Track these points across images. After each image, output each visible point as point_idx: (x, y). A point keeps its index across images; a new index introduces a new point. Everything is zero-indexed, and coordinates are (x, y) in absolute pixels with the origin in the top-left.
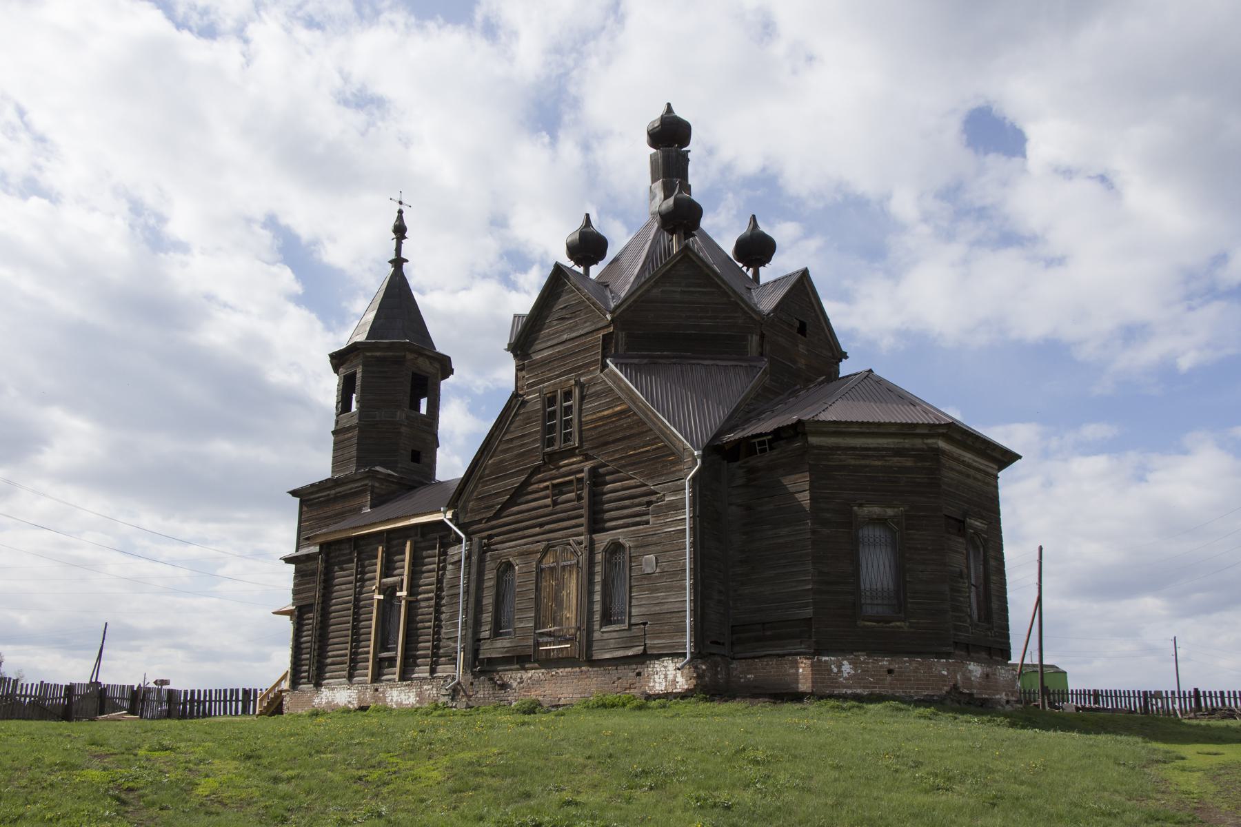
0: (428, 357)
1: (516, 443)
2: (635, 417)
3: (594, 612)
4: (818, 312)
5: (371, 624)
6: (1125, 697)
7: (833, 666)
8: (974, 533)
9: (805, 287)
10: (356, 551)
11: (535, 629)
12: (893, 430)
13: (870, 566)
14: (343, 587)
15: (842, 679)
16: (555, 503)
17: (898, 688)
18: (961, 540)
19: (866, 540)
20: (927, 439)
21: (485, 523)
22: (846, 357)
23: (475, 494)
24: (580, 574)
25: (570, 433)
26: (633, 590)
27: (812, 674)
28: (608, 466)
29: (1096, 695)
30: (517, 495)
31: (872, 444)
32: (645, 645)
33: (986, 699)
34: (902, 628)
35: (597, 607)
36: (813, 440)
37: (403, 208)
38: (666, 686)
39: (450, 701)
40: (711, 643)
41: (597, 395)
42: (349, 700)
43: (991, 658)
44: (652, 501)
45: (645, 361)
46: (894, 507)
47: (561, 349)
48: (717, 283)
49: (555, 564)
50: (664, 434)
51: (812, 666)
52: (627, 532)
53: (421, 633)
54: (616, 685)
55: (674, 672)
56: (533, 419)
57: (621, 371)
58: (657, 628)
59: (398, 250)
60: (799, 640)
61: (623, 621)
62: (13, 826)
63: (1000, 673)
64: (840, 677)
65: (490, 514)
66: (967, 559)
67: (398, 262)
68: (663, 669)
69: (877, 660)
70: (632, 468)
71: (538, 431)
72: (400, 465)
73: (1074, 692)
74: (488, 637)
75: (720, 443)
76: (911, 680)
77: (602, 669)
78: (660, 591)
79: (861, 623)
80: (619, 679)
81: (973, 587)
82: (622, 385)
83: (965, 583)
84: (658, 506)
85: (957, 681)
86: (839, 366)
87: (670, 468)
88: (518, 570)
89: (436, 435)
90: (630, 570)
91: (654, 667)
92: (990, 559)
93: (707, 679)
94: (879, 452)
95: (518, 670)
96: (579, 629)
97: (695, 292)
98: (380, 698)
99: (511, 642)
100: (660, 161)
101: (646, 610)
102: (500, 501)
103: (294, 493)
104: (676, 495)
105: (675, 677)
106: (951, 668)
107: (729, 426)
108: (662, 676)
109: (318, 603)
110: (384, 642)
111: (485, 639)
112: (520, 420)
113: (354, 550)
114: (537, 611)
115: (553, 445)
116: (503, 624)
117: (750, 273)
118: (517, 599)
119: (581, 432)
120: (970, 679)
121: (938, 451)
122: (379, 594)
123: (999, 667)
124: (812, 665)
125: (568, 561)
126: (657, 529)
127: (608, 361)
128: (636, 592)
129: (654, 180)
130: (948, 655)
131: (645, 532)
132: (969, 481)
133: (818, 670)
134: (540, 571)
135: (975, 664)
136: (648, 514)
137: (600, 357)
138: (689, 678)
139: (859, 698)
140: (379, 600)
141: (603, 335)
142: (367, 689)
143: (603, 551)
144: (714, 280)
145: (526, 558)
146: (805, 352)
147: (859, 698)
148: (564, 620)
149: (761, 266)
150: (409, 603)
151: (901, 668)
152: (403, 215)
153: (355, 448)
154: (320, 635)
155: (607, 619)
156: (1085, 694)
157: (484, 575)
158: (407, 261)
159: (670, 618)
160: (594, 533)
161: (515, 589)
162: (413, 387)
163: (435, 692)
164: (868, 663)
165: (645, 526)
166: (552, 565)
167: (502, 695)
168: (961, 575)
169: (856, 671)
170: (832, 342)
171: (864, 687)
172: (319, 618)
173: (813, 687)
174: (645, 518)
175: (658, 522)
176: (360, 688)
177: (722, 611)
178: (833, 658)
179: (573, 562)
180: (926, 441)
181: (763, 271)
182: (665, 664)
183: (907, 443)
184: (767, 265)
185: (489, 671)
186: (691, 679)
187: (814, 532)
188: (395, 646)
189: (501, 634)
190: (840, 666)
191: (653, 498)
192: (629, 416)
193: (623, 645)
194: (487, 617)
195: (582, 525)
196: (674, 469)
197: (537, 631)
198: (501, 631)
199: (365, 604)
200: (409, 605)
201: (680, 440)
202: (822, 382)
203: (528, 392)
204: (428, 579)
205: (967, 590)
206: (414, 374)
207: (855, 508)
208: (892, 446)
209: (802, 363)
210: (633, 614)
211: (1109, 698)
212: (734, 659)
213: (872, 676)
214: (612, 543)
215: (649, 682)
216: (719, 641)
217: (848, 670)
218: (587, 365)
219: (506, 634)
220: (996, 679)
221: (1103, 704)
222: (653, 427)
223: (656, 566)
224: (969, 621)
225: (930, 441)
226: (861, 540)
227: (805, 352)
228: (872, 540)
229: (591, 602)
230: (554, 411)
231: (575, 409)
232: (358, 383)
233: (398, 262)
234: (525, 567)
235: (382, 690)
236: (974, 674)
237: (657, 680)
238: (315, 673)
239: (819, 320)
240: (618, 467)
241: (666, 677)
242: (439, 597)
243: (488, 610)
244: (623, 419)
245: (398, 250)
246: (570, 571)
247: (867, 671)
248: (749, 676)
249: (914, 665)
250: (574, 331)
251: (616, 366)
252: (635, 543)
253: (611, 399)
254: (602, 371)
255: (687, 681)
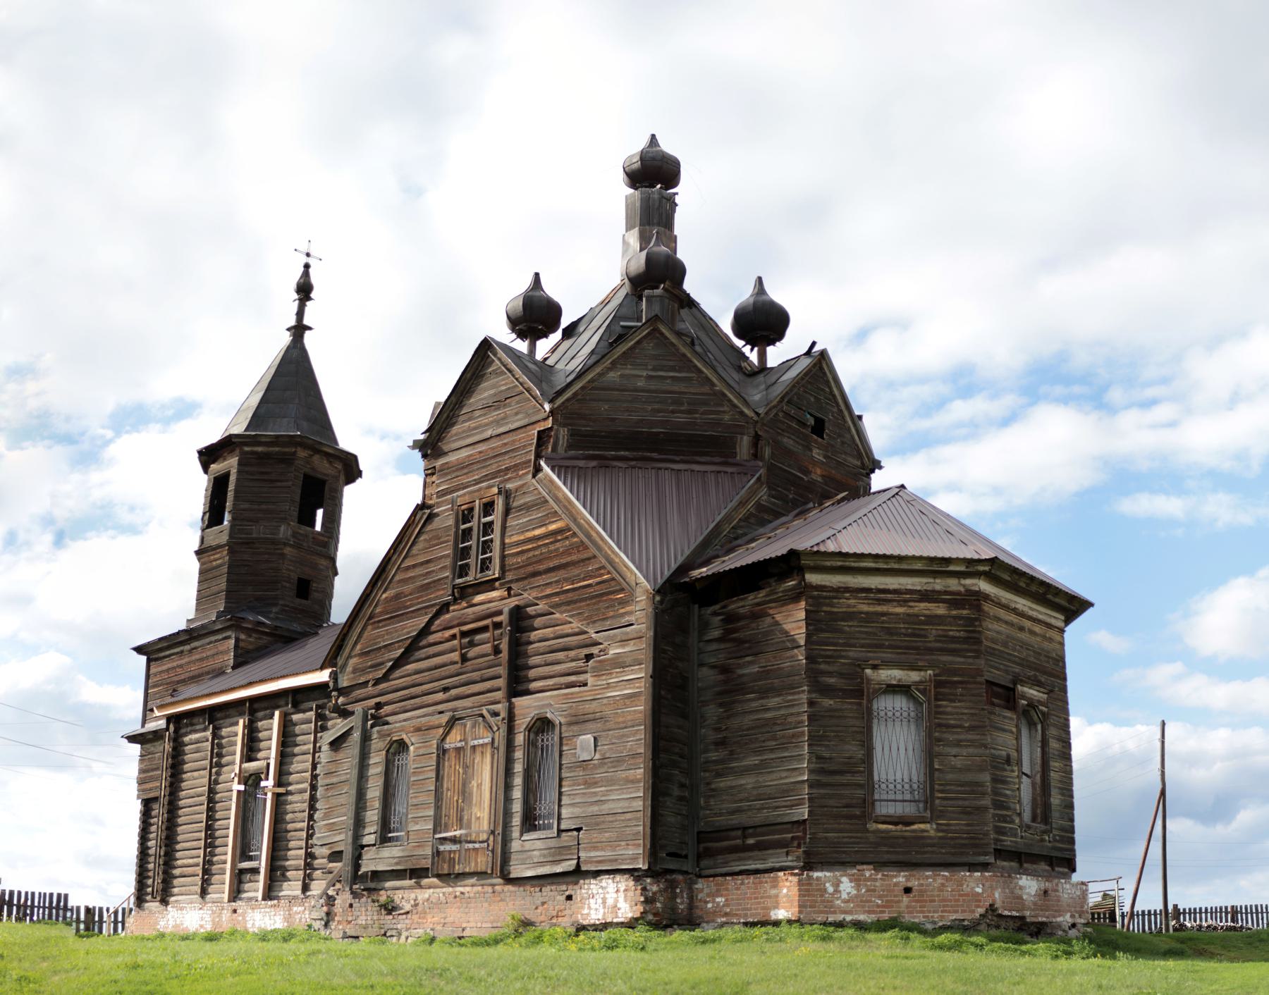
0: (327, 455)
1: (418, 571)
2: (576, 539)
3: (512, 813)
4: (843, 407)
5: (229, 824)
6: (1252, 913)
7: (827, 885)
8: (1028, 705)
9: (825, 374)
10: (211, 726)
11: (435, 832)
12: (918, 566)
13: (887, 749)
14: (196, 774)
15: (839, 902)
16: (464, 659)
17: (917, 912)
18: (1008, 714)
19: (882, 714)
20: (964, 578)
21: (374, 685)
22: (880, 468)
23: (358, 647)
24: (496, 756)
25: (490, 559)
26: (564, 783)
27: (799, 896)
28: (538, 605)
29: (1235, 912)
30: (412, 647)
31: (891, 584)
32: (579, 858)
33: (1043, 924)
34: (927, 831)
35: (517, 807)
36: (813, 578)
37: (311, 261)
38: (604, 913)
39: (322, 928)
40: (667, 855)
41: (527, 508)
42: (202, 923)
43: (1053, 870)
44: (592, 654)
45: (594, 463)
46: (920, 670)
47: (484, 448)
48: (696, 366)
49: (463, 743)
50: (611, 562)
51: (799, 885)
52: (558, 696)
53: (292, 836)
54: (539, 911)
55: (615, 895)
56: (441, 540)
57: (559, 477)
58: (595, 835)
59: (300, 314)
60: (785, 850)
61: (549, 827)
62: (370, 993)
63: (1063, 889)
64: (838, 899)
65: (380, 674)
66: (1017, 739)
67: (299, 330)
68: (600, 891)
69: (887, 876)
70: (568, 608)
71: (446, 556)
72: (281, 602)
73: (1209, 910)
74: (373, 843)
75: (687, 580)
76: (934, 901)
77: (522, 889)
78: (600, 784)
79: (872, 826)
80: (543, 903)
81: (1024, 777)
82: (560, 495)
83: (1013, 771)
84: (600, 661)
85: (994, 900)
86: (870, 479)
87: (618, 610)
88: (414, 752)
89: (333, 560)
90: (561, 756)
91: (589, 889)
92: (1050, 740)
93: (658, 905)
94: (899, 596)
95: (411, 888)
96: (493, 832)
97: (666, 378)
98: (239, 922)
99: (403, 850)
100: (638, 204)
101: (581, 810)
102: (392, 657)
103: (139, 650)
104: (623, 646)
105: (616, 901)
106: (987, 884)
107: (701, 555)
108: (600, 901)
109: (164, 796)
110: (244, 850)
111: (369, 846)
112: (425, 540)
113: (209, 724)
114: (438, 808)
115: (467, 575)
116: (392, 826)
117: (753, 356)
118: (411, 792)
119: (503, 557)
120: (1020, 898)
121: (980, 596)
122: (239, 783)
123: (1063, 881)
124: (800, 883)
125: (479, 738)
126: (597, 692)
127: (542, 463)
128: (569, 786)
129: (629, 227)
130: (984, 866)
131: (581, 697)
132: (1023, 636)
133: (808, 890)
134: (442, 752)
135: (1029, 878)
136: (586, 672)
137: (533, 458)
138: (633, 903)
139: (860, 926)
140: (239, 792)
141: (539, 432)
142: (223, 909)
143: (525, 729)
144: (691, 361)
145: (424, 735)
146: (821, 458)
147: (860, 926)
148: (473, 819)
149: (769, 345)
150: (277, 796)
151: (922, 885)
152: (311, 270)
153: (225, 580)
154: (167, 838)
155: (530, 822)
156: (1201, 913)
157: (369, 758)
158: (310, 328)
159: (612, 822)
160: (515, 697)
161: (409, 777)
162: (304, 496)
163: (307, 916)
164: (876, 880)
165: (582, 689)
166: (459, 745)
167: (389, 922)
168: (1008, 760)
169: (858, 890)
170: (860, 447)
171: (869, 912)
172: (166, 815)
173: (800, 912)
174: (581, 678)
175: (599, 683)
176: (214, 908)
177: (684, 812)
178: (828, 874)
179: (486, 741)
180: (963, 581)
181: (770, 350)
182: (604, 884)
183: (939, 584)
184: (778, 344)
185: (375, 890)
186: (636, 905)
187: (811, 703)
188: (258, 853)
189: (390, 840)
190: (837, 885)
191: (595, 650)
192: (567, 538)
193: (551, 859)
194: (372, 816)
195: (499, 689)
196: (622, 611)
197: (438, 836)
198: (390, 835)
199: (222, 797)
200: (277, 800)
201: (632, 572)
202: (843, 499)
203: (437, 503)
204: (301, 765)
205: (1017, 780)
206: (306, 476)
207: (868, 671)
208: (919, 588)
209: (817, 474)
210: (563, 816)
211: (1249, 915)
212: (700, 876)
213: (880, 897)
214: (538, 719)
215: (583, 908)
216: (679, 852)
217: (849, 890)
218: (516, 467)
219: (397, 839)
220: (1059, 896)
221: (1242, 922)
222: (597, 553)
223: (595, 750)
224: (1017, 821)
225: (968, 582)
226: (875, 714)
227: (821, 458)
228: (890, 714)
229: (508, 800)
230: (470, 529)
231: (497, 528)
232: (231, 487)
233: (299, 330)
234: (424, 747)
235: (241, 911)
236: (1027, 891)
237: (593, 906)
238: (161, 886)
239: (843, 417)
240: (551, 607)
241: (604, 902)
242: (314, 787)
243: (373, 806)
244: (559, 541)
245: (300, 314)
246: (482, 753)
247: (874, 891)
248: (718, 900)
249: (939, 881)
250: (502, 425)
251: (553, 469)
252: (568, 719)
253: (544, 514)
254: (534, 476)
255: (631, 907)
